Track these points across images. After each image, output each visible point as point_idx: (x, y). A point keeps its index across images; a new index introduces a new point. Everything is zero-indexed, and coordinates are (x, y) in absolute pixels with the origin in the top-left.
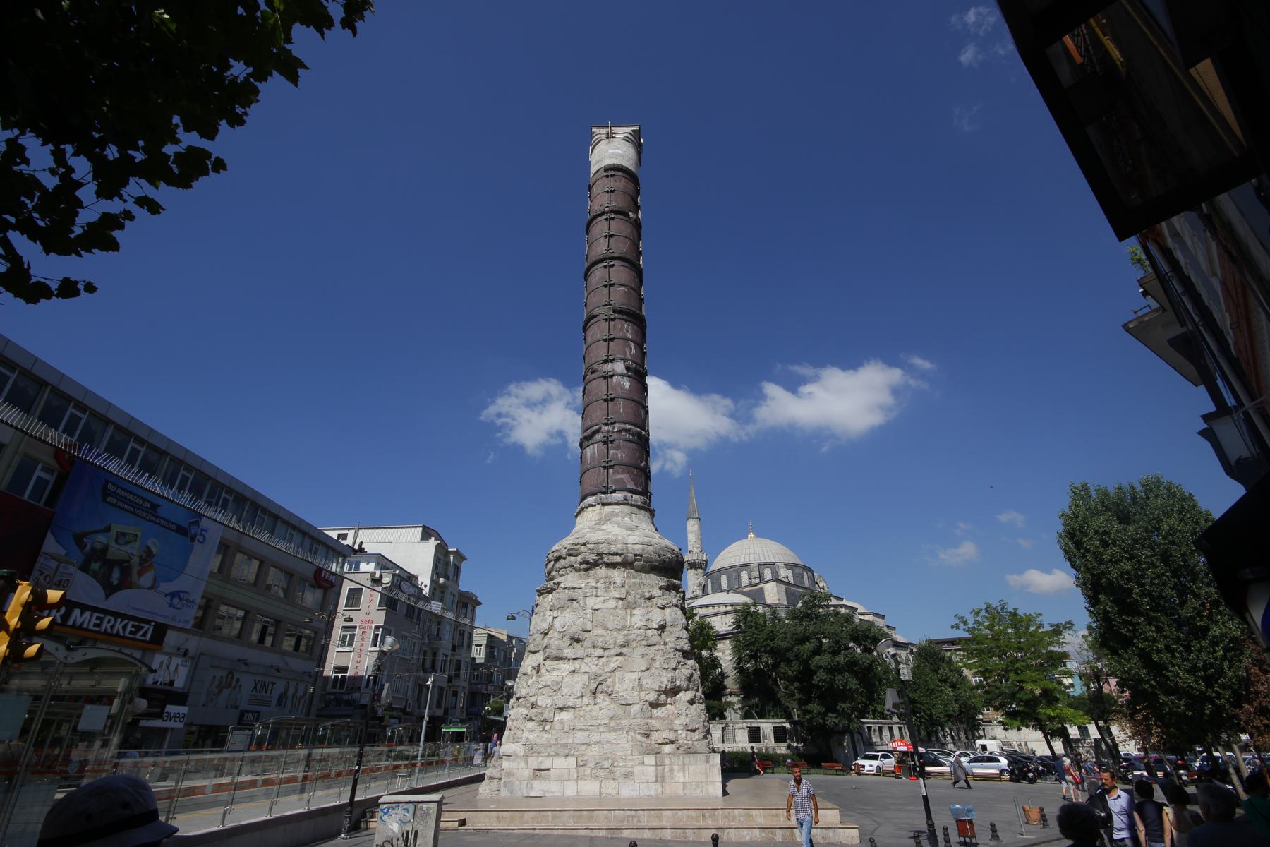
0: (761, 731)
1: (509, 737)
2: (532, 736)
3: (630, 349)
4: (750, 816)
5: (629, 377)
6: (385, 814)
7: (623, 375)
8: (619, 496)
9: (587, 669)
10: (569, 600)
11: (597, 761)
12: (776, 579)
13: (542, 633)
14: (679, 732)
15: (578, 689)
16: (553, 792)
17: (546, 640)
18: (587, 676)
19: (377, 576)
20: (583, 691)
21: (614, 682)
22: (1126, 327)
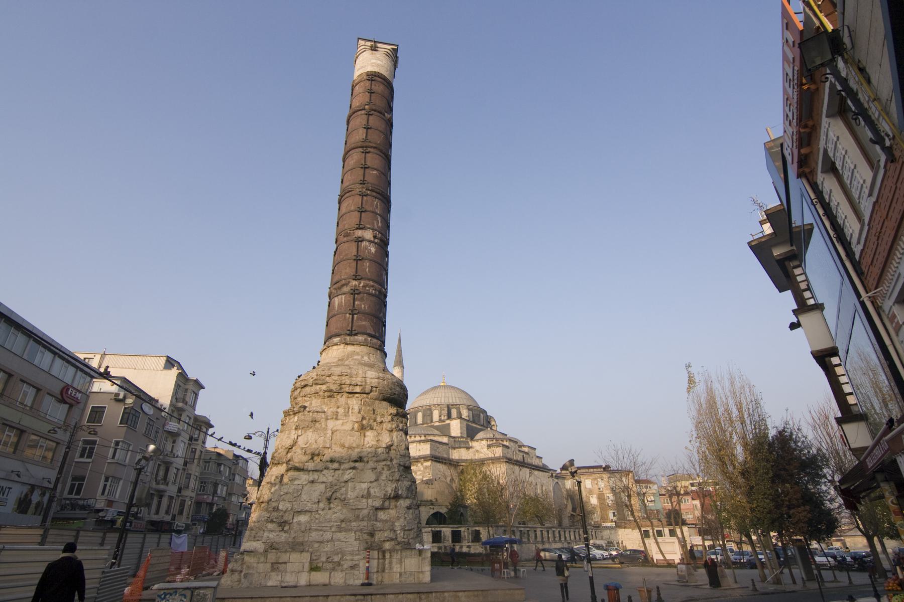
0: (442, 534)
1: (250, 536)
3: (378, 221)
4: (458, 597)
5: (376, 243)
6: (163, 599)
7: (370, 242)
8: (360, 338)
9: (324, 479)
10: (312, 422)
11: (329, 556)
12: (460, 417)
13: (286, 448)
14: (398, 532)
15: (315, 496)
16: (287, 582)
17: (289, 455)
18: (322, 487)
19: (121, 397)
20: (320, 497)
21: (347, 490)
22: (749, 243)
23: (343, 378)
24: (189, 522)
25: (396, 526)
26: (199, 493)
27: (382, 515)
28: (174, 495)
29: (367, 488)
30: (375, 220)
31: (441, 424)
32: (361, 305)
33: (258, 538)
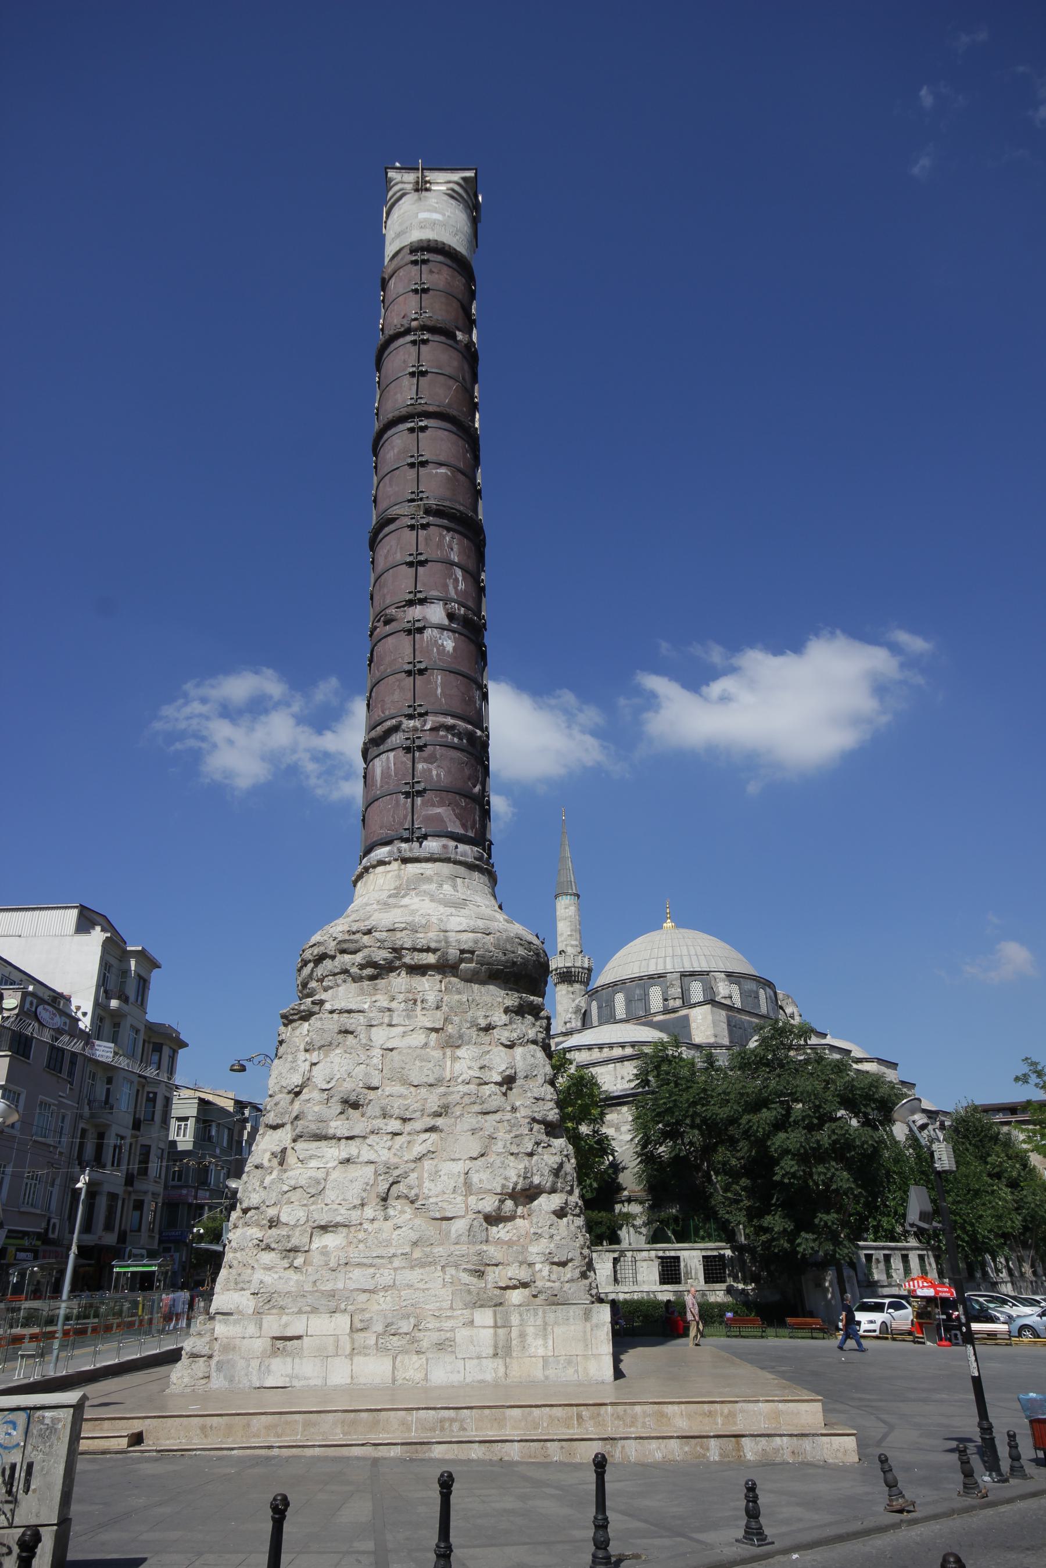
0: (682, 1264)
1: (227, 1280)
2: (269, 1278)
3: (456, 580)
4: (662, 1415)
5: (453, 631)
7: (442, 628)
8: (432, 845)
9: (372, 1157)
14: (538, 1267)
15: (354, 1194)
17: (297, 1105)
18: (371, 1168)
20: (364, 1195)
21: (420, 1178)
23: (399, 935)
24: (156, 1247)
25: (532, 1254)
26: (171, 1183)
27: (500, 1232)
28: (120, 1190)
29: (462, 1171)
30: (450, 577)
31: (667, 1017)
32: (430, 770)
33: (241, 1285)
